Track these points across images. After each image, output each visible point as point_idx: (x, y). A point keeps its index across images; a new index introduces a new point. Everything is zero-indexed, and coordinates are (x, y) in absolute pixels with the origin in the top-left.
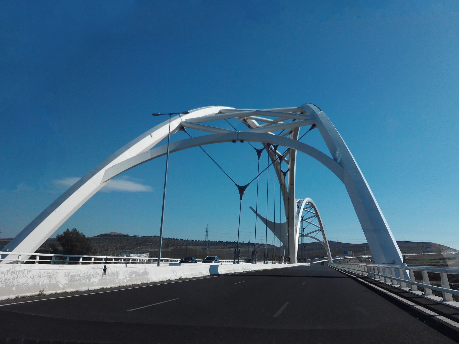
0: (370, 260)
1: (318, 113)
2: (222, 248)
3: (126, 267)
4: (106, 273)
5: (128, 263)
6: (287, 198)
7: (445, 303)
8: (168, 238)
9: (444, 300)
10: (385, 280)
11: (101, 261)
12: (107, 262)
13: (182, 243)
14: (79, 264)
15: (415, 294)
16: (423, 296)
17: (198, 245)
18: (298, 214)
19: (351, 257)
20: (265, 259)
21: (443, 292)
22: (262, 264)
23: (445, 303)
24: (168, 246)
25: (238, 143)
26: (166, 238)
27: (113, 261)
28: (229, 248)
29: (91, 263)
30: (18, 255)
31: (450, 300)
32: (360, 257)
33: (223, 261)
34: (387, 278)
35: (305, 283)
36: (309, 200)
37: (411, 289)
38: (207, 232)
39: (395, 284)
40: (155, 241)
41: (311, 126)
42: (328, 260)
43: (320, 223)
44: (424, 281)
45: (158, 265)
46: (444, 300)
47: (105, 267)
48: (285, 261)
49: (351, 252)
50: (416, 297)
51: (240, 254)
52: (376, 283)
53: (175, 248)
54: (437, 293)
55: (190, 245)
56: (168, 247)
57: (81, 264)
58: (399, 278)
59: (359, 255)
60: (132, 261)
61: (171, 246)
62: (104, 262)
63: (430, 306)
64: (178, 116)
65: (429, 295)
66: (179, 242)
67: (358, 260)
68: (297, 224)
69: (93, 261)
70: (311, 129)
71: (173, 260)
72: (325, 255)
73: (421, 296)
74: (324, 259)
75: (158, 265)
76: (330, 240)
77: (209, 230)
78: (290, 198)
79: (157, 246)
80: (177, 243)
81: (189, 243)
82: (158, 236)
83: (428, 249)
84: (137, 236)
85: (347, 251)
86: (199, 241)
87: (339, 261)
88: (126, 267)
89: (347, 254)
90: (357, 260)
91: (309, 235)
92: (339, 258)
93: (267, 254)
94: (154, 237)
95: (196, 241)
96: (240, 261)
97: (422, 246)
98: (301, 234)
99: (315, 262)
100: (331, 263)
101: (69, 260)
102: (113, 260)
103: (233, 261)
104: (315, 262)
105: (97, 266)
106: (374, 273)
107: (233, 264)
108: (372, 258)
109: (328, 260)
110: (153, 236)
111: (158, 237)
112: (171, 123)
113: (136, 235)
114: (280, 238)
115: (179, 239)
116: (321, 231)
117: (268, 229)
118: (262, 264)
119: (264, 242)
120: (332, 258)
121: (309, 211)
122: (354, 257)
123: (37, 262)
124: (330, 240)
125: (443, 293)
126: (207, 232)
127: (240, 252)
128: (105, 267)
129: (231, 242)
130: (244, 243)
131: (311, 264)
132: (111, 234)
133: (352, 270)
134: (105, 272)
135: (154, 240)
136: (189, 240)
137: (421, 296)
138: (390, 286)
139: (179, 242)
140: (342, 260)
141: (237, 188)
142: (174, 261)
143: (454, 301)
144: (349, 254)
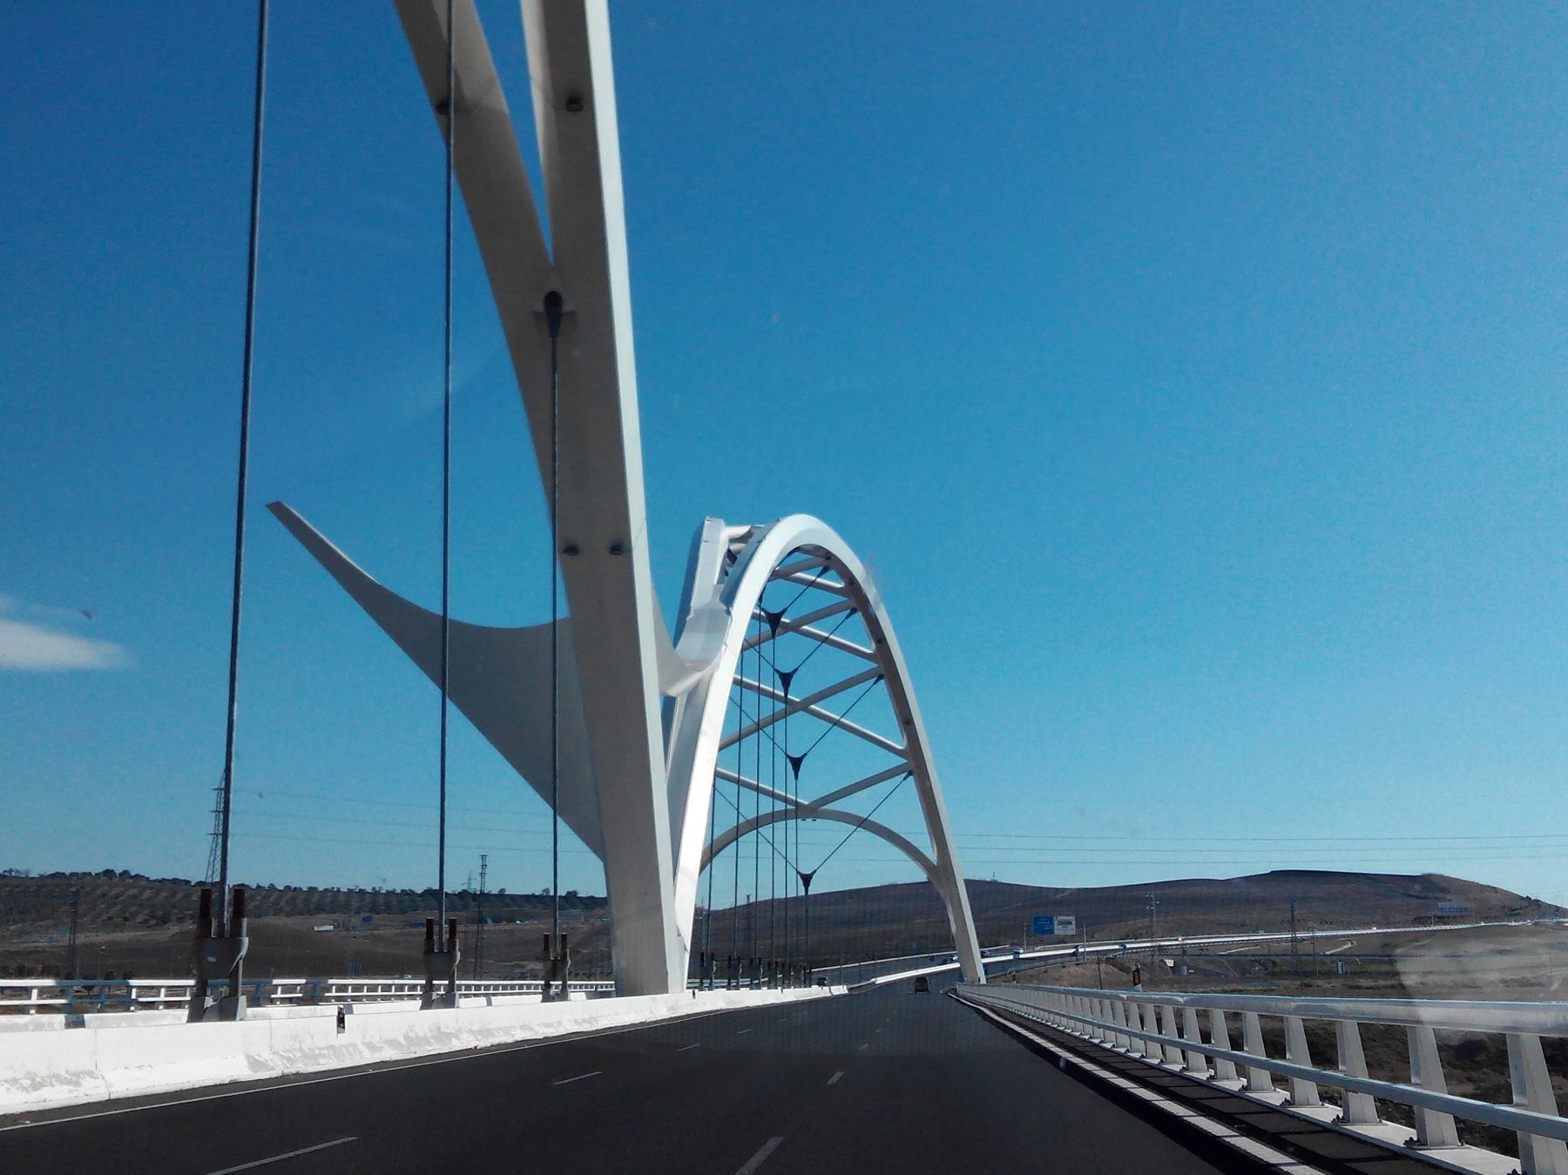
4: (344, 1027)
8: (175, 881)
9: (1422, 1142)
15: (1441, 1168)
16: (1410, 1153)
17: (320, 909)
18: (729, 597)
21: (1519, 1133)
22: (694, 994)
24: (164, 921)
26: (163, 880)
32: (1117, 947)
37: (1188, 1066)
39: (1308, 1104)
44: (1418, 1075)
45: (489, 1003)
50: (1220, 1098)
52: (1166, 1082)
54: (1392, 1109)
55: (278, 912)
56: (166, 923)
57: (33, 1011)
59: (1108, 939)
61: (180, 920)
65: (1442, 1144)
67: (1108, 961)
75: (489, 1003)
78: (567, 306)
79: (110, 918)
81: (274, 904)
83: (1440, 905)
84: (18, 871)
85: (1051, 920)
86: (326, 890)
89: (1051, 931)
91: (832, 806)
92: (1011, 957)
95: (312, 890)
96: (569, 982)
97: (1401, 891)
98: (786, 800)
99: (880, 980)
100: (975, 982)
101: (38, 999)
102: (35, 992)
104: (880, 980)
106: (1160, 1033)
108: (1181, 952)
110: (101, 871)
111: (120, 874)
112: (755, 815)
113: (11, 871)
116: (911, 777)
118: (694, 994)
121: (825, 640)
122: (1088, 949)
125: (1415, 1108)
131: (850, 990)
134: (342, 1025)
135: (99, 892)
137: (1327, 1126)
138: (1279, 1112)
142: (163, 990)
143: (1462, 1145)
144: (1059, 930)
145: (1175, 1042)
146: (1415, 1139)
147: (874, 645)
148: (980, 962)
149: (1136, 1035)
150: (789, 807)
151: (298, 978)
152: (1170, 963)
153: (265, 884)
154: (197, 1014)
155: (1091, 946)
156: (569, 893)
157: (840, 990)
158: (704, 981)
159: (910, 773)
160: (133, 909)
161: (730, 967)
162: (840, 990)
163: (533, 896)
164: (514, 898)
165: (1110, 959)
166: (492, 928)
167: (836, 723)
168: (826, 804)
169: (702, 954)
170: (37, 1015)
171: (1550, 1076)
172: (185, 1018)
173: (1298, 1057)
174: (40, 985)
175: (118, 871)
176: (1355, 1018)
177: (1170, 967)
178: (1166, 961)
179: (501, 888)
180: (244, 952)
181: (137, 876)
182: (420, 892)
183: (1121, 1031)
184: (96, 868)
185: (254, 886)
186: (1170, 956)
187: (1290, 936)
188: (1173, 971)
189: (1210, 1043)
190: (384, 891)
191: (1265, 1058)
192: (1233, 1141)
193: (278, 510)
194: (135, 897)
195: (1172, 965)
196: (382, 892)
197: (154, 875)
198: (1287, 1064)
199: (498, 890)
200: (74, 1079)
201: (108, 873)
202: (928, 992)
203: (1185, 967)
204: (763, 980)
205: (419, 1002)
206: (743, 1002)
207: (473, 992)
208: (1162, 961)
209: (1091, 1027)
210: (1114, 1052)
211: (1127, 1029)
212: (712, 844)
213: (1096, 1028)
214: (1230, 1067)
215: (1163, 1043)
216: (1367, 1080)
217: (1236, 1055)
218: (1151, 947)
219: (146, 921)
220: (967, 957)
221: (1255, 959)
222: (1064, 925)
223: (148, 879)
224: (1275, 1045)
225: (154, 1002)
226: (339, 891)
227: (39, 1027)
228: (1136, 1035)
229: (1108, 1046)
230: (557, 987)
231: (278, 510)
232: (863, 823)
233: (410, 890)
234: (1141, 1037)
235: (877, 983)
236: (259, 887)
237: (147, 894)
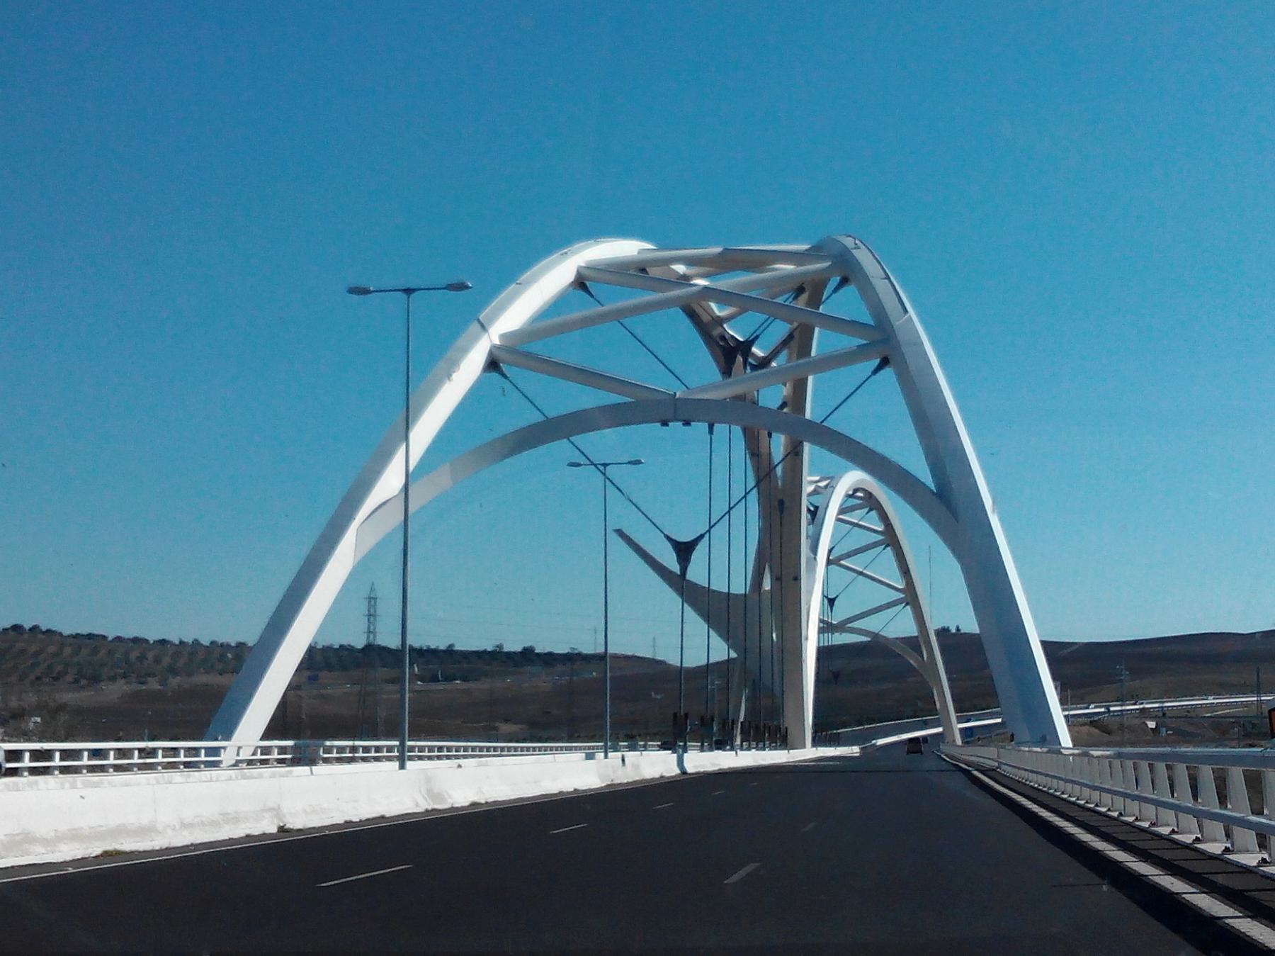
0: (1152, 725)
1: (897, 323)
5: (16, 769)
6: (776, 503)
8: (90, 636)
11: (48, 761)
13: (166, 660)
14: (52, 774)
24: (95, 679)
25: (676, 426)
26: (77, 636)
27: (57, 762)
29: (369, 759)
30: (237, 748)
32: (1103, 710)
33: (387, 746)
36: (862, 481)
37: (1232, 845)
38: (372, 619)
40: (23, 652)
41: (877, 362)
42: (940, 730)
43: (905, 571)
45: (402, 767)
48: (748, 740)
51: (689, 727)
53: (135, 687)
58: (411, 665)
59: (1097, 702)
60: (62, 759)
61: (113, 679)
64: (475, 327)
66: (150, 655)
67: (1093, 724)
68: (810, 593)
70: (876, 371)
71: (107, 751)
72: (924, 709)
74: (925, 725)
75: (402, 767)
76: (958, 629)
78: (787, 503)
79: (38, 678)
80: (142, 658)
87: (997, 735)
90: (1084, 724)
91: (856, 625)
94: (12, 633)
95: (163, 642)
99: (881, 742)
102: (27, 755)
104: (881, 742)
105: (211, 775)
108: (1161, 714)
109: (940, 730)
111: (30, 630)
114: (726, 636)
115: (147, 641)
117: (687, 608)
120: (960, 720)
123: (55, 768)
124: (958, 629)
127: (688, 721)
130: (500, 652)
131: (861, 749)
133: (1077, 788)
136: (206, 642)
139: (150, 655)
141: (669, 546)
145: (1216, 814)
147: (883, 527)
149: (1187, 811)
150: (825, 626)
151: (599, 742)
153: (189, 639)
157: (855, 750)
159: (907, 604)
160: (59, 668)
162: (855, 750)
163: (485, 652)
164: (466, 655)
167: (861, 573)
170: (61, 776)
174: (164, 746)
175: (27, 626)
177: (1152, 729)
179: (450, 643)
181: (49, 631)
185: (177, 643)
186: (1151, 719)
187: (1255, 699)
188: (1153, 732)
193: (620, 533)
194: (55, 655)
195: (1154, 727)
196: (318, 647)
197: (67, 631)
199: (447, 645)
200: (805, 756)
202: (922, 753)
203: (1164, 729)
206: (719, 765)
208: (1144, 722)
209: (1110, 796)
210: (1196, 850)
211: (1171, 800)
212: (407, 429)
213: (1128, 801)
214: (1250, 838)
215: (1199, 815)
216: (1218, 811)
218: (1158, 707)
220: (948, 726)
221: (1237, 721)
223: (61, 634)
225: (48, 767)
228: (1187, 811)
229: (1165, 831)
231: (620, 533)
233: (349, 645)
235: (878, 744)
236: (182, 643)
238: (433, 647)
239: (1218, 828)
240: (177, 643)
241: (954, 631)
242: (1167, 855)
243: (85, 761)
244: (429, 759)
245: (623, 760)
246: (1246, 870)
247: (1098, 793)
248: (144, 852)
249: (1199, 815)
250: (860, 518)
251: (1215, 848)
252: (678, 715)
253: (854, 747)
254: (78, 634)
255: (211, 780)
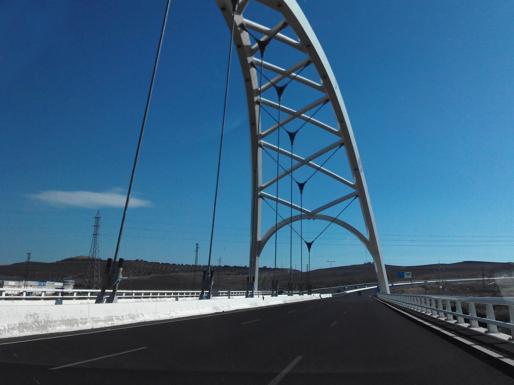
2: (227, 275)
3: (259, 297)
7: (471, 328)
8: (155, 263)
10: (438, 314)
12: (64, 297)
16: (486, 334)
19: (411, 283)
20: (289, 289)
23: (471, 328)
24: (150, 273)
28: (236, 274)
30: (41, 292)
31: (436, 314)
34: (441, 312)
35: (336, 322)
37: (439, 316)
39: (462, 323)
45: (229, 298)
46: (488, 332)
47: (263, 297)
49: (410, 274)
54: (482, 324)
62: (62, 297)
63: (474, 337)
65: (450, 320)
67: (422, 286)
69: (89, 296)
71: (189, 293)
73: (508, 342)
75: (177, 300)
77: (101, 223)
82: (140, 260)
85: (403, 273)
88: (259, 297)
90: (419, 287)
93: (277, 281)
96: (118, 291)
99: (348, 292)
100: (385, 293)
102: (89, 294)
103: (246, 291)
104: (348, 292)
107: (96, 302)
110: (135, 260)
115: (170, 264)
119: (287, 266)
122: (415, 283)
126: (97, 226)
128: (263, 297)
129: (240, 267)
132: (79, 259)
133: (401, 303)
137: (506, 341)
140: (395, 288)
143: (499, 332)
146: (511, 338)
147: (322, 82)
148: (388, 285)
150: (303, 213)
152: (441, 287)
153: (180, 264)
154: (201, 298)
155: (417, 282)
156: (264, 267)
157: (329, 295)
158: (290, 291)
159: (357, 196)
161: (248, 283)
162: (329, 295)
165: (423, 286)
166: (242, 276)
167: (318, 169)
168: (319, 212)
169: (300, 284)
171: (509, 315)
172: (54, 304)
173: (459, 312)
175: (140, 260)
176: (449, 300)
178: (440, 287)
180: (212, 285)
182: (223, 266)
183: (415, 305)
184: (134, 259)
185: (177, 265)
186: (440, 285)
189: (438, 308)
190: (213, 266)
191: (477, 317)
192: (432, 326)
198: (511, 324)
201: (137, 260)
204: (304, 292)
205: (245, 296)
207: (242, 294)
208: (438, 286)
211: (426, 306)
216: (477, 317)
217: (444, 311)
219: (145, 274)
222: (408, 275)
223: (148, 262)
224: (465, 311)
225: (86, 297)
226: (201, 266)
227: (185, 300)
230: (250, 292)
232: (334, 220)
234: (421, 306)
235: (347, 293)
236: (178, 264)
237: (147, 266)
238: (241, 266)
239: (436, 312)
240: (177, 265)
241: (372, 263)
242: (415, 314)
243: (143, 296)
244: (25, 300)
245: (263, 298)
246: (442, 321)
247: (411, 305)
248: (241, 309)
249: (432, 309)
250: (298, 73)
251: (435, 316)
252: (207, 272)
253: (324, 297)
254: (152, 262)
255: (184, 300)
